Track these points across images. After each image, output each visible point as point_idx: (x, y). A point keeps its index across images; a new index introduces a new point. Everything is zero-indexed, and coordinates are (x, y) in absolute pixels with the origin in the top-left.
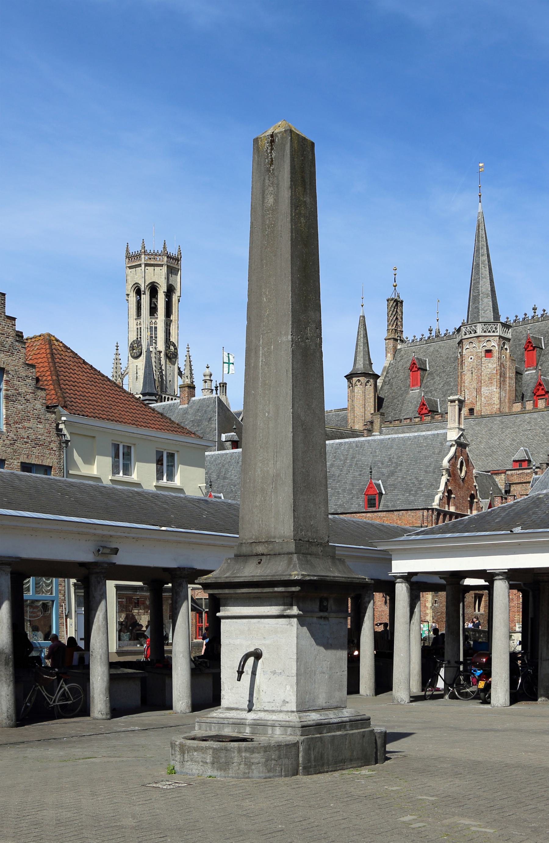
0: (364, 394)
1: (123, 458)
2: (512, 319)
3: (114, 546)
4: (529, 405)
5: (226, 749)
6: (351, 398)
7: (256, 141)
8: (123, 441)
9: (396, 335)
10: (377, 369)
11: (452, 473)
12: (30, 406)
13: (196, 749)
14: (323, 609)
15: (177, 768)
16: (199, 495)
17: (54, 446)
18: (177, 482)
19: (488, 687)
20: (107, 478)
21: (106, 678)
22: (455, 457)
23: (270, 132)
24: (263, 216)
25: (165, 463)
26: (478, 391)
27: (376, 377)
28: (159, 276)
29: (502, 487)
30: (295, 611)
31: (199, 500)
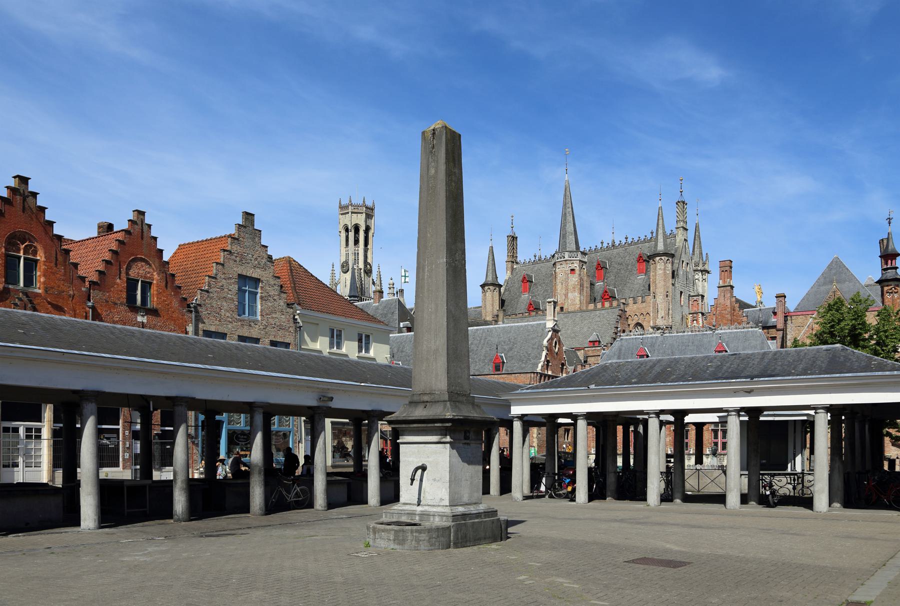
0: (492, 297)
1: (336, 338)
2: (587, 249)
3: (330, 395)
4: (599, 305)
5: (403, 531)
6: (484, 300)
7: (423, 133)
8: (337, 327)
10: (501, 281)
12: (276, 304)
13: (383, 531)
14: (466, 438)
15: (371, 543)
16: (386, 362)
17: (292, 330)
18: (372, 354)
19: (574, 490)
20: (326, 351)
21: (324, 483)
22: (551, 339)
23: (432, 128)
24: (428, 181)
25: (364, 341)
26: (566, 295)
27: (500, 286)
28: (360, 220)
29: (582, 358)
30: (448, 439)
31: (386, 366)
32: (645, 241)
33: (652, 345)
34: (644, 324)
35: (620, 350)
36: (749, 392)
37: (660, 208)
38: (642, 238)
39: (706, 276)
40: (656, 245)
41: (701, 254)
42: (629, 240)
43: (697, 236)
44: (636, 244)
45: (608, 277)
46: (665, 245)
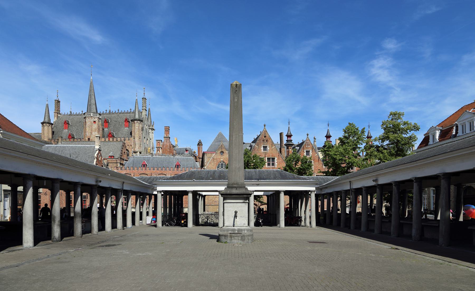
0: (48, 129)
2: (102, 112)
6: (43, 130)
7: (231, 85)
9: (58, 111)
10: (52, 122)
11: (97, 159)
15: (228, 241)
22: (98, 154)
23: (235, 83)
26: (91, 133)
27: (52, 124)
32: (127, 113)
33: (148, 161)
34: (129, 150)
35: (134, 162)
36: (258, 185)
37: (137, 100)
38: (126, 111)
39: (153, 131)
40: (135, 116)
41: (151, 121)
42: (120, 111)
43: (149, 114)
44: (123, 113)
45: (110, 127)
46: (139, 116)
